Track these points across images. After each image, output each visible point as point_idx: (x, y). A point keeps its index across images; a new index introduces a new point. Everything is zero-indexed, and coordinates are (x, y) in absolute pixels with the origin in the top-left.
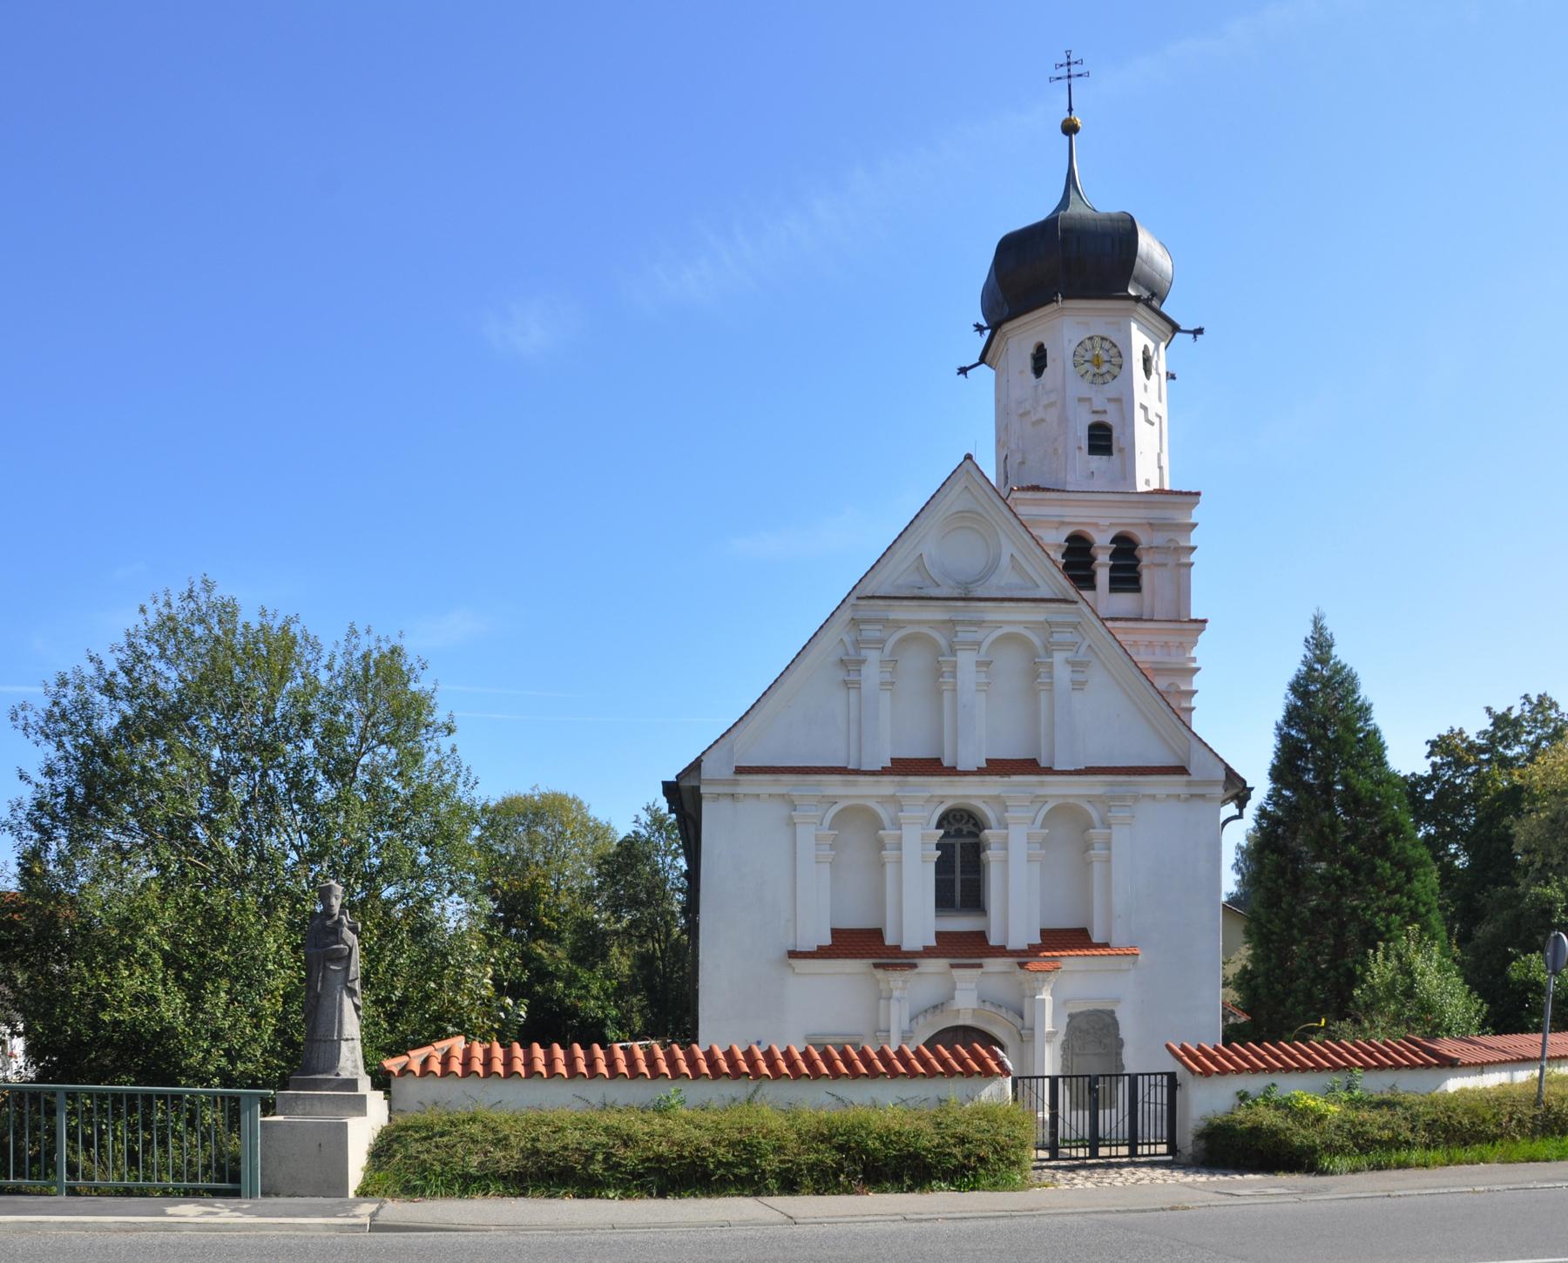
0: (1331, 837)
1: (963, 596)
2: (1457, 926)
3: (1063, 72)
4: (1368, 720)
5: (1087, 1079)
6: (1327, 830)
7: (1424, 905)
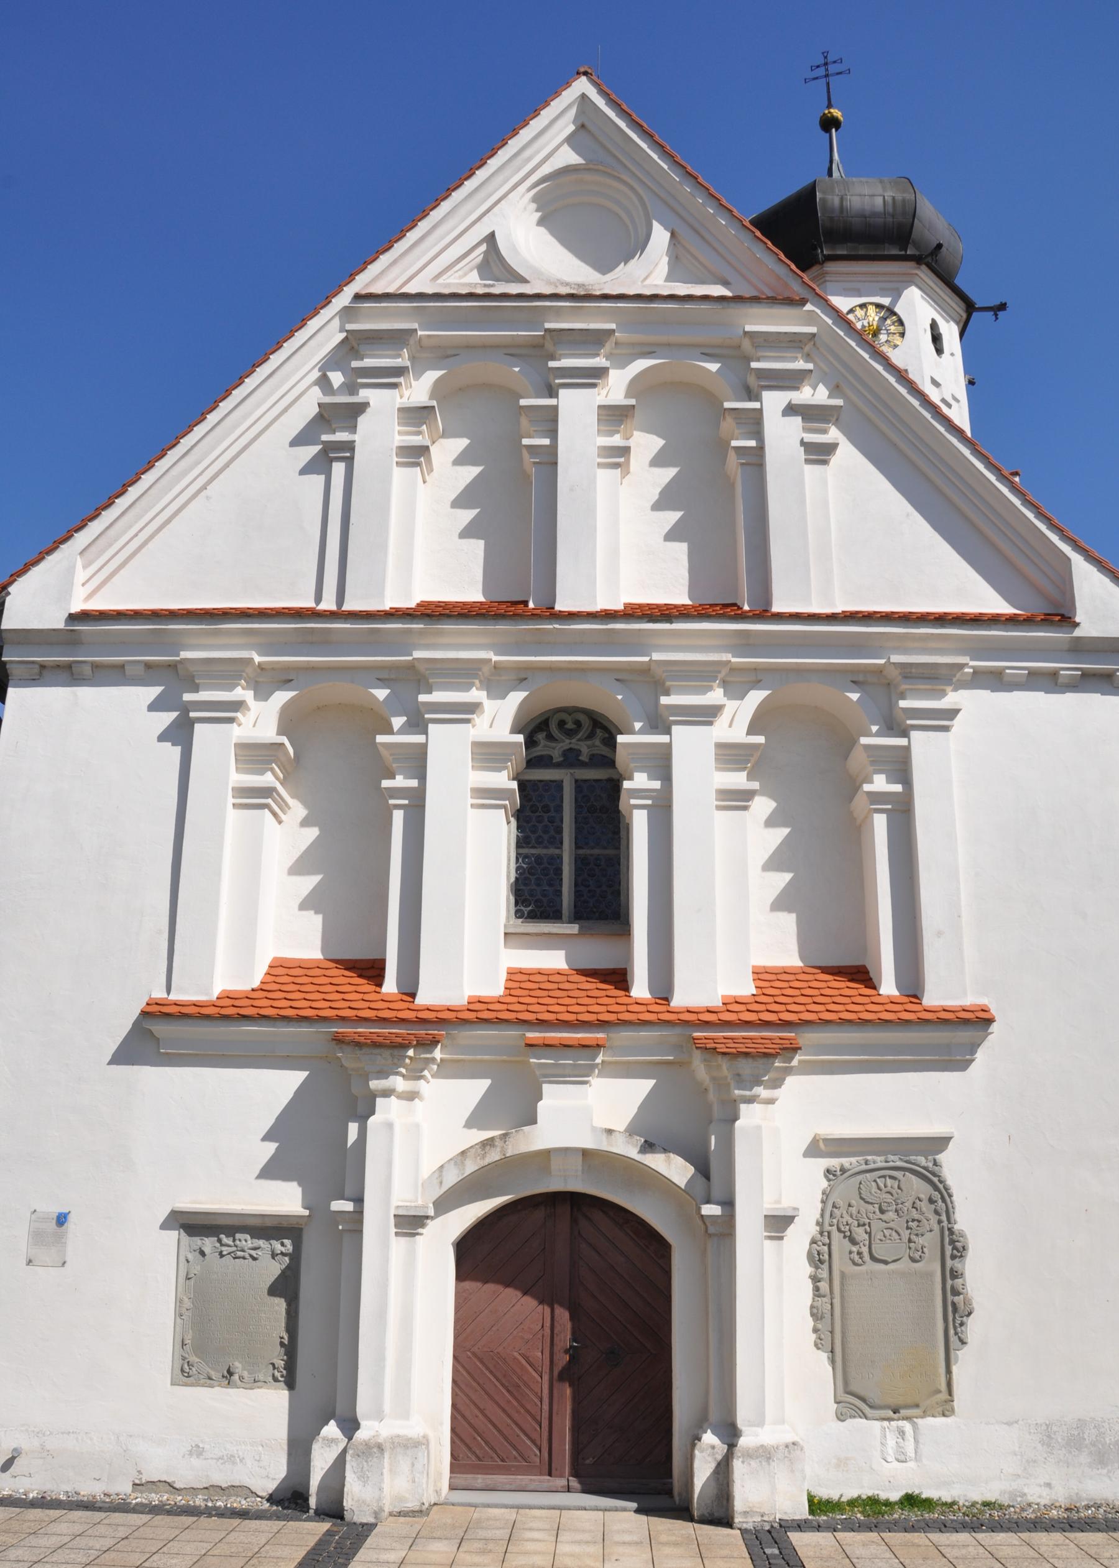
3: (821, 72)
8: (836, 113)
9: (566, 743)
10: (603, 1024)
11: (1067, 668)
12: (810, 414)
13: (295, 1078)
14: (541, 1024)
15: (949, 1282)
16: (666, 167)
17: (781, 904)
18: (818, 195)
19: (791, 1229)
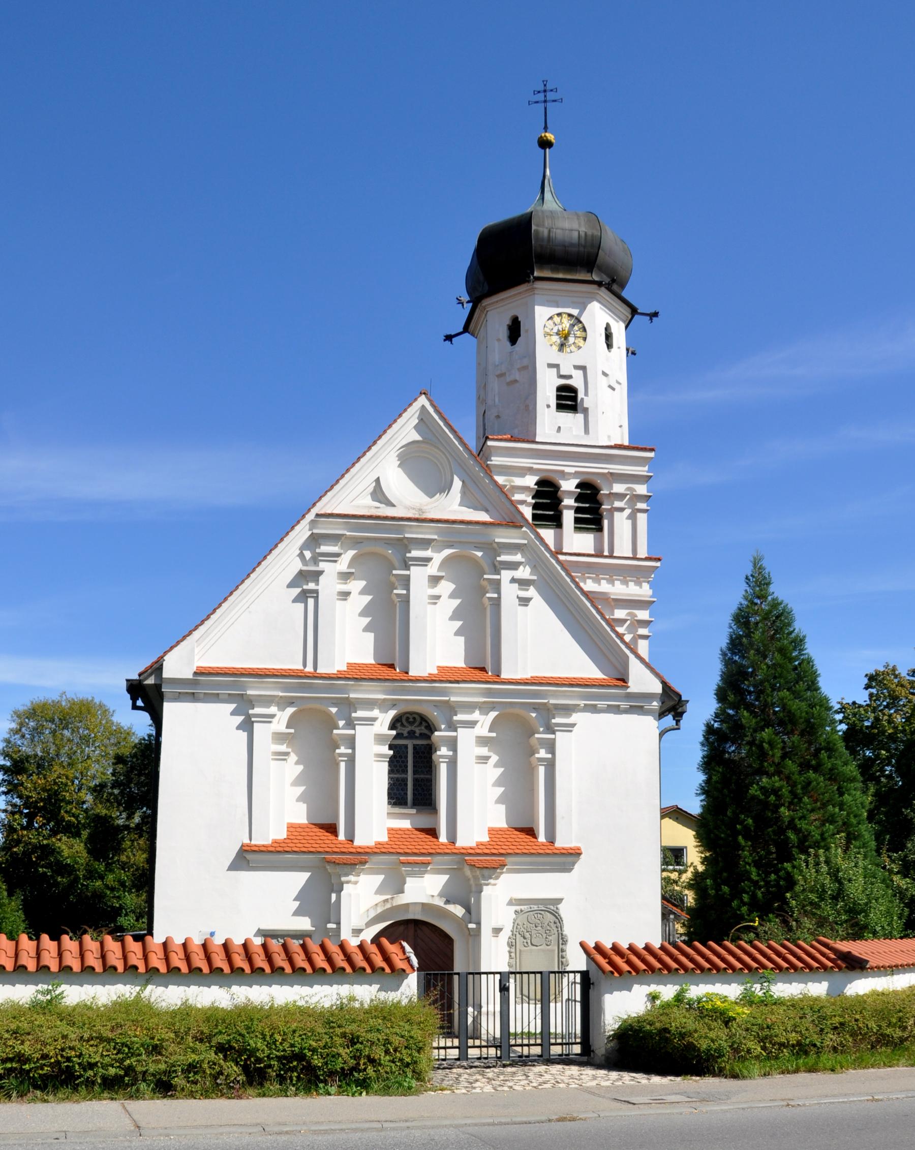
0: (744, 742)
1: (417, 516)
2: (888, 837)
3: (541, 97)
4: (803, 650)
5: (498, 977)
6: (766, 746)
7: (855, 816)
8: (550, 136)
9: (410, 728)
10: (430, 854)
11: (624, 705)
12: (523, 583)
13: (306, 875)
14: (406, 854)
15: (560, 954)
16: (461, 449)
17: (499, 801)
18: (534, 227)
19: (501, 933)
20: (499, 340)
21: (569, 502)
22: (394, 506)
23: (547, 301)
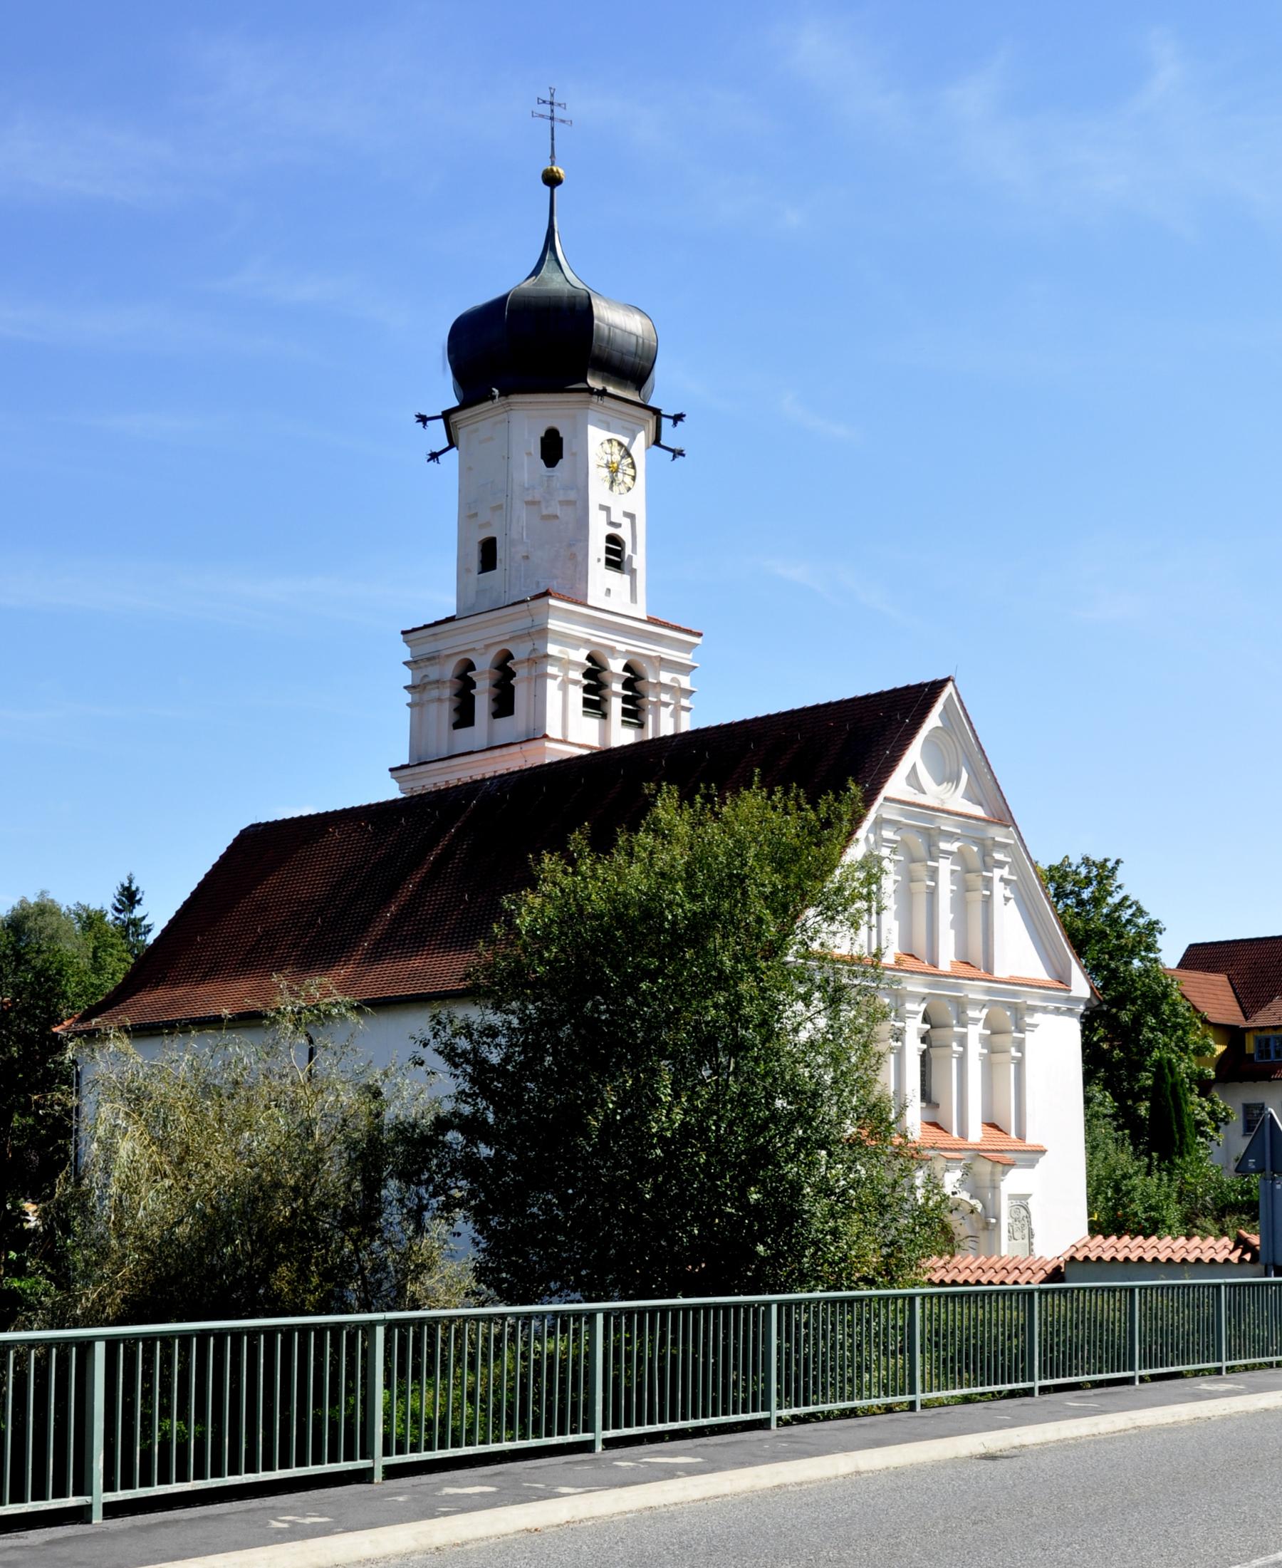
1: (940, 806)
3: (546, 109)
20: (529, 454)
21: (617, 687)
22: (924, 793)
23: (623, 427)
